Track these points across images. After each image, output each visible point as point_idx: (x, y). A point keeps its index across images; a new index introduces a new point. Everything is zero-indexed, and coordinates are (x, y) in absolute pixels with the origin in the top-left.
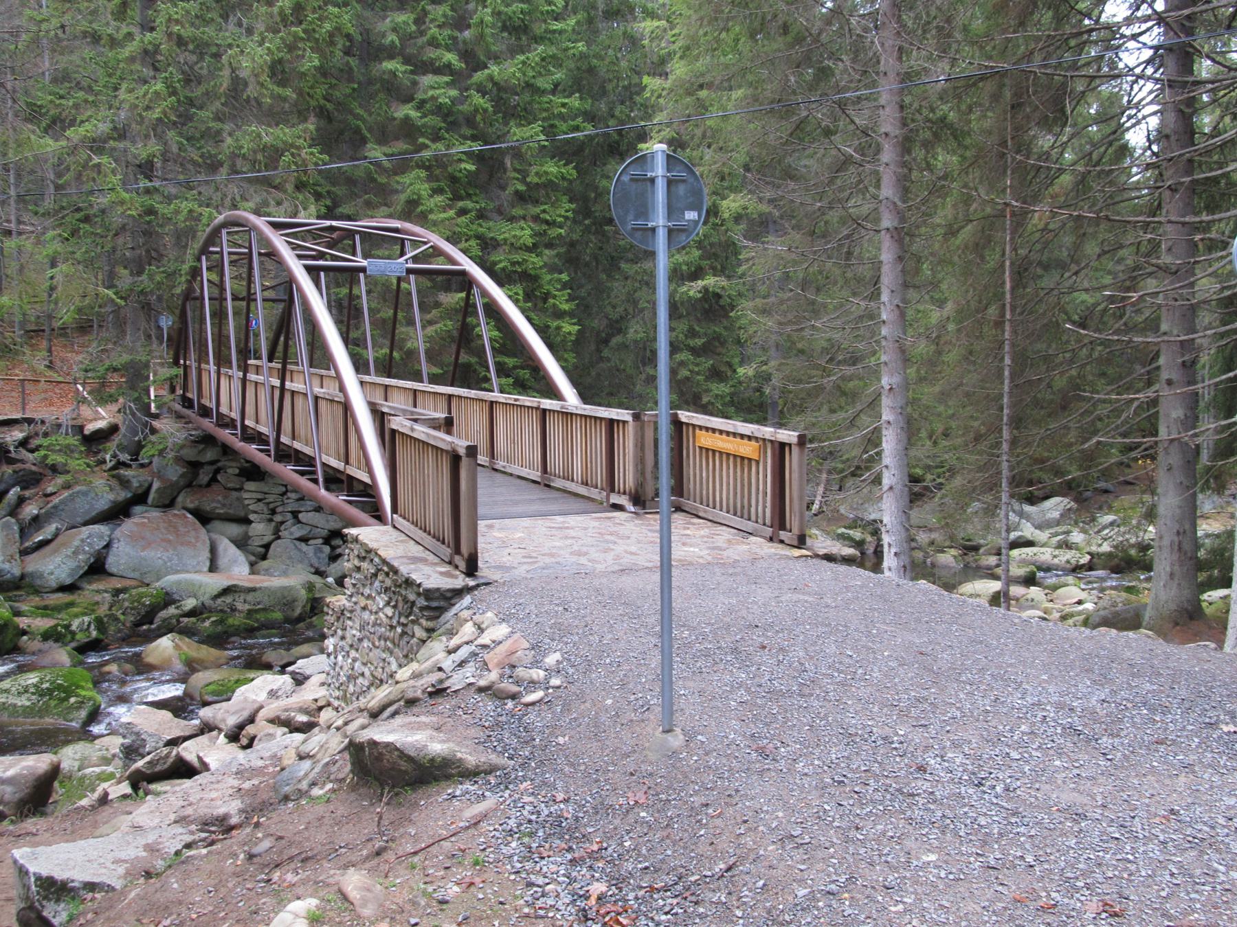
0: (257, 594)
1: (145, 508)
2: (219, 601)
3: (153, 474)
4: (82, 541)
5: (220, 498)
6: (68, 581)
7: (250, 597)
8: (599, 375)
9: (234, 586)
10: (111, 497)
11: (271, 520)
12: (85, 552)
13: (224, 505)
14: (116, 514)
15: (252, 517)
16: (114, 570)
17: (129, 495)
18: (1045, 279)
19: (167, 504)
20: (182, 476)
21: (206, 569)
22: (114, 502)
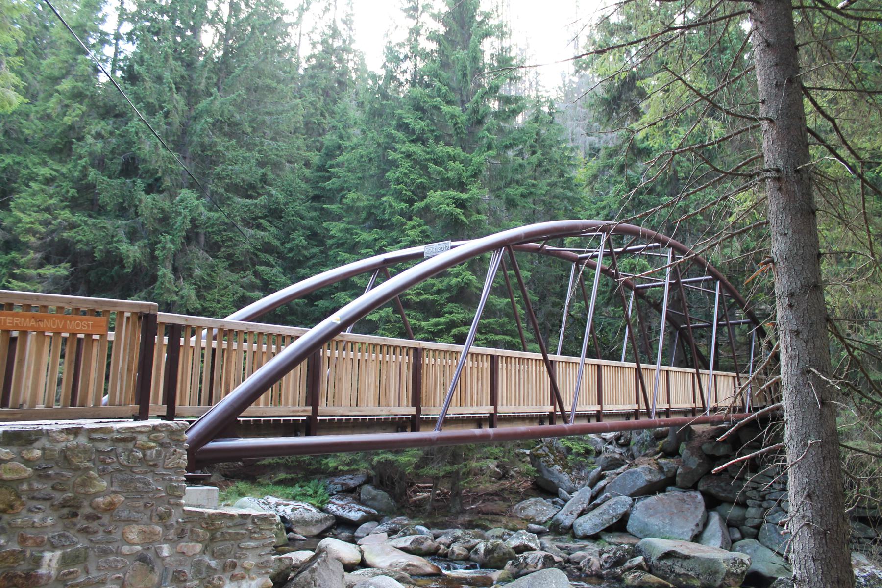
0: (691, 562)
1: (674, 488)
2: (663, 562)
3: (679, 463)
4: (609, 506)
5: (722, 484)
6: (591, 532)
7: (685, 564)
8: (319, 98)
9: (674, 552)
10: (648, 477)
11: (760, 506)
12: (608, 514)
13: (725, 490)
14: (650, 490)
15: (749, 502)
16: (360, 558)
17: (663, 478)
18: (774, 570)
19: (685, 488)
20: (699, 465)
21: (688, 538)
22: (649, 481)
